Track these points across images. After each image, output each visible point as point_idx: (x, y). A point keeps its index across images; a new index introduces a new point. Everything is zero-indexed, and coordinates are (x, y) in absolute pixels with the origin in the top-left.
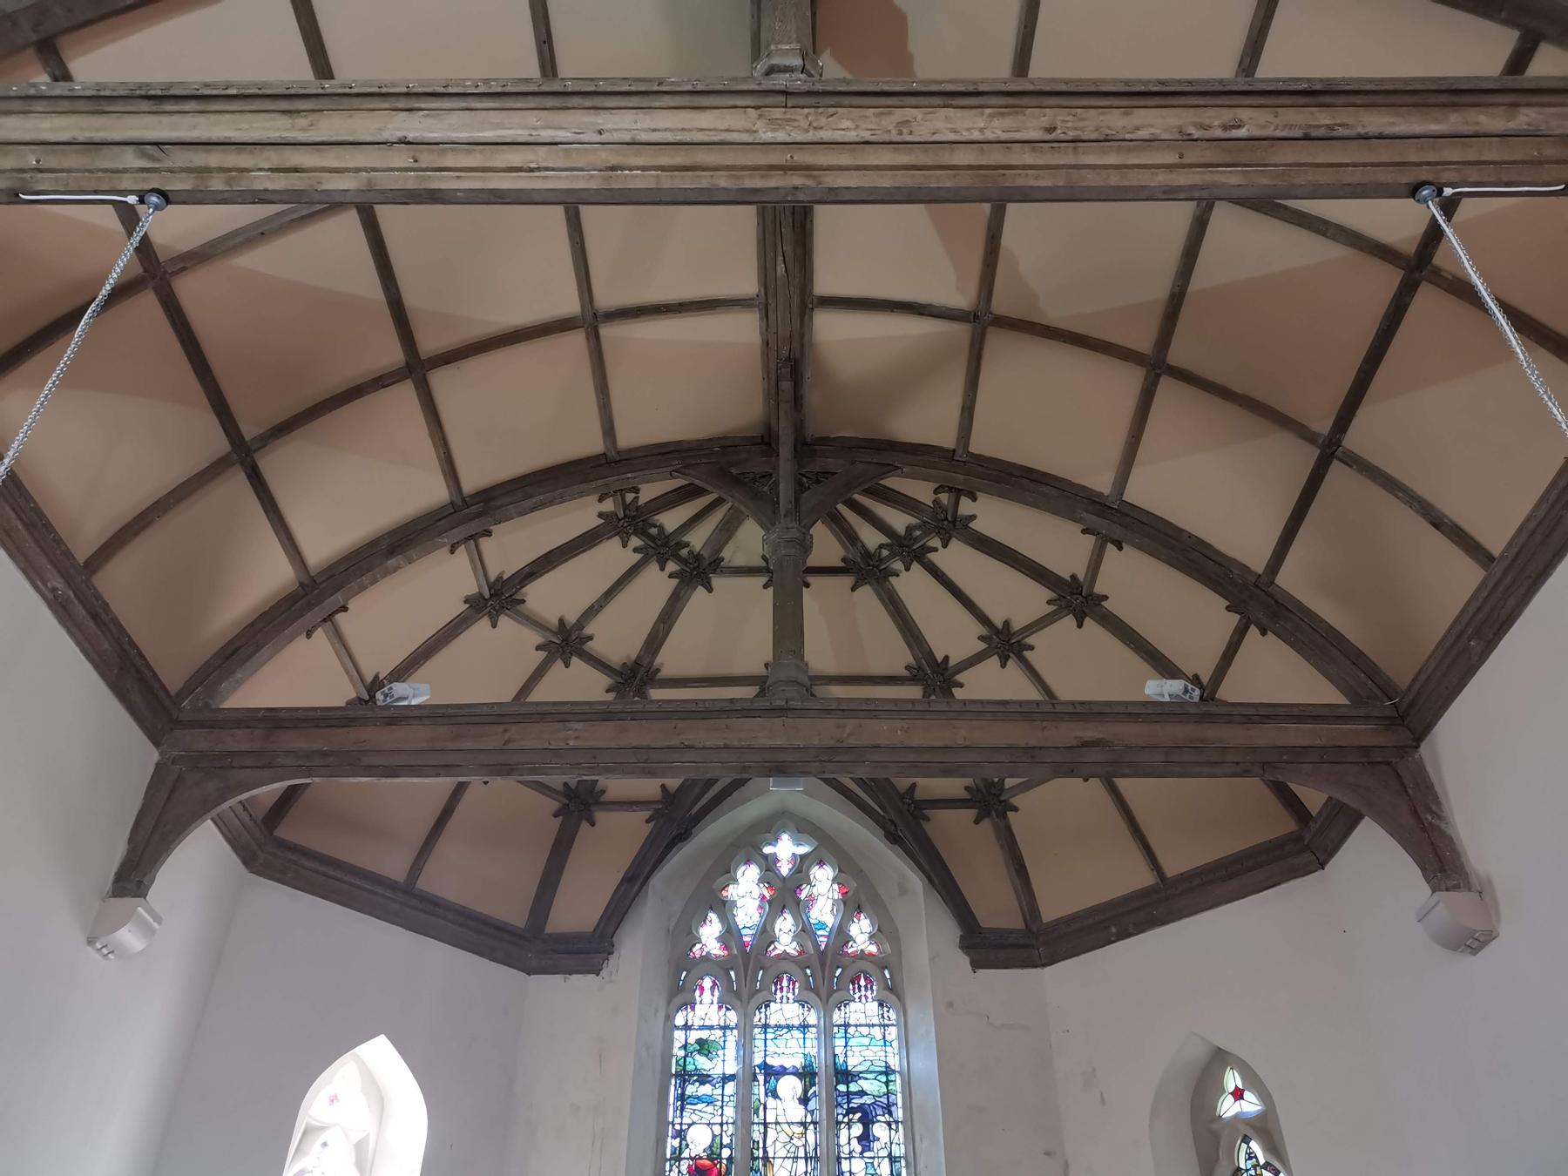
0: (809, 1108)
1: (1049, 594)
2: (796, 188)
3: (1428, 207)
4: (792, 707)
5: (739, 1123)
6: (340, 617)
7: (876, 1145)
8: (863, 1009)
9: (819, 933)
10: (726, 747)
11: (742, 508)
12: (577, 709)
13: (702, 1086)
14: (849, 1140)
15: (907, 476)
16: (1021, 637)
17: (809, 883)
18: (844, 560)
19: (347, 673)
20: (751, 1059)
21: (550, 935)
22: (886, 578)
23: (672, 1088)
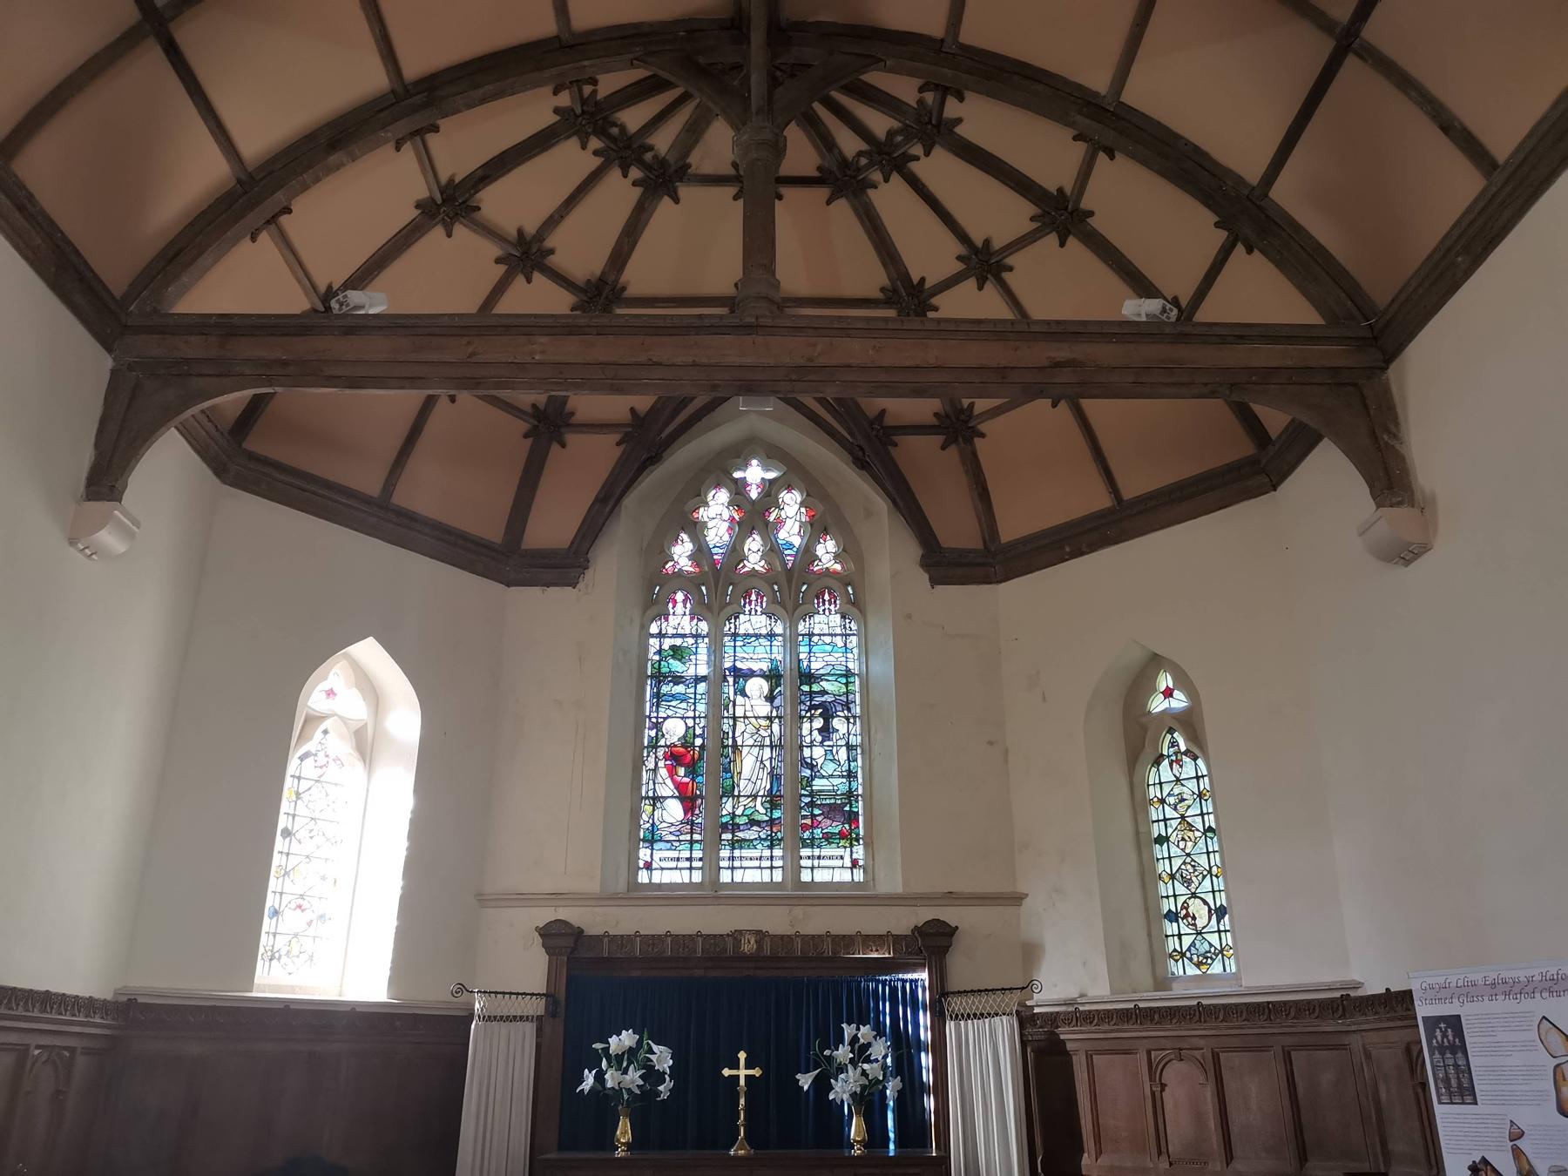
4: (761, 324)
5: (710, 717)
6: (284, 220)
7: (835, 736)
8: (826, 621)
9: (786, 552)
10: (695, 364)
11: (711, 105)
13: (676, 687)
14: (811, 732)
16: (1001, 256)
17: (778, 507)
20: (722, 663)
21: (526, 551)
23: (648, 688)
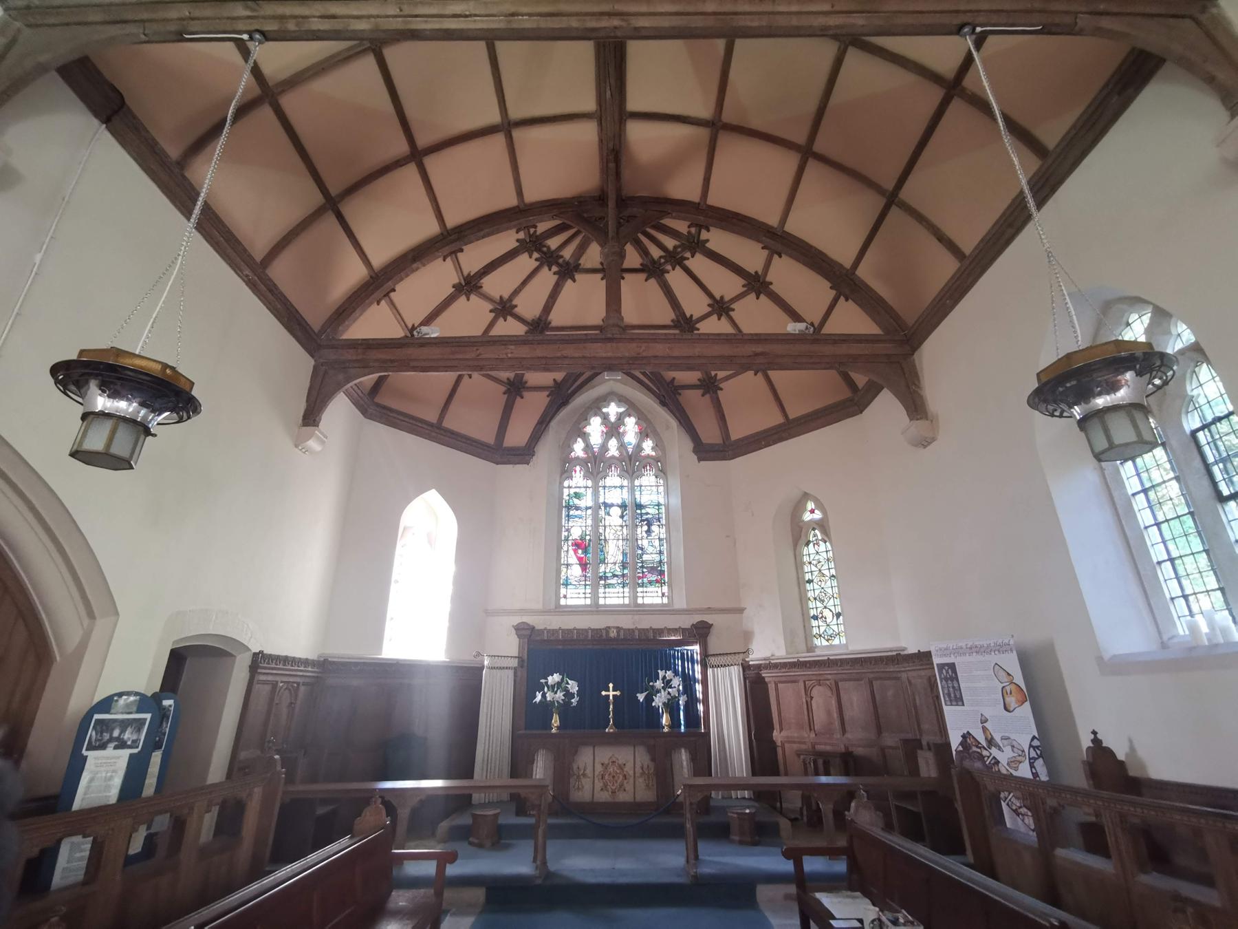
0: (624, 519)
1: (743, 282)
2: (615, 28)
3: (966, 39)
6: (392, 294)
7: (653, 534)
8: (648, 479)
11: (591, 236)
12: (512, 339)
15: (675, 218)
18: (641, 265)
19: (399, 323)
21: (505, 447)
22: (662, 275)
